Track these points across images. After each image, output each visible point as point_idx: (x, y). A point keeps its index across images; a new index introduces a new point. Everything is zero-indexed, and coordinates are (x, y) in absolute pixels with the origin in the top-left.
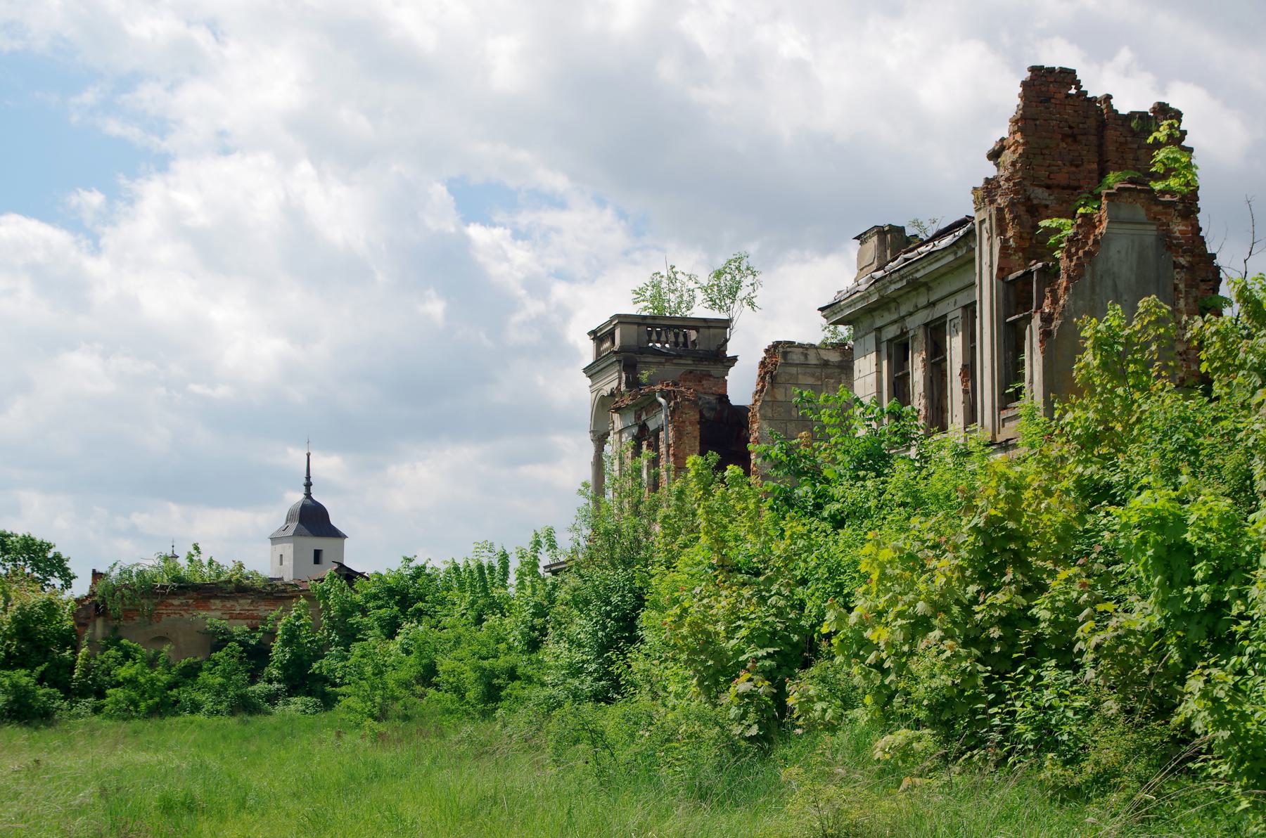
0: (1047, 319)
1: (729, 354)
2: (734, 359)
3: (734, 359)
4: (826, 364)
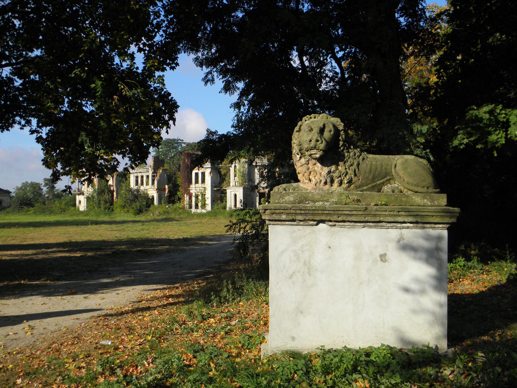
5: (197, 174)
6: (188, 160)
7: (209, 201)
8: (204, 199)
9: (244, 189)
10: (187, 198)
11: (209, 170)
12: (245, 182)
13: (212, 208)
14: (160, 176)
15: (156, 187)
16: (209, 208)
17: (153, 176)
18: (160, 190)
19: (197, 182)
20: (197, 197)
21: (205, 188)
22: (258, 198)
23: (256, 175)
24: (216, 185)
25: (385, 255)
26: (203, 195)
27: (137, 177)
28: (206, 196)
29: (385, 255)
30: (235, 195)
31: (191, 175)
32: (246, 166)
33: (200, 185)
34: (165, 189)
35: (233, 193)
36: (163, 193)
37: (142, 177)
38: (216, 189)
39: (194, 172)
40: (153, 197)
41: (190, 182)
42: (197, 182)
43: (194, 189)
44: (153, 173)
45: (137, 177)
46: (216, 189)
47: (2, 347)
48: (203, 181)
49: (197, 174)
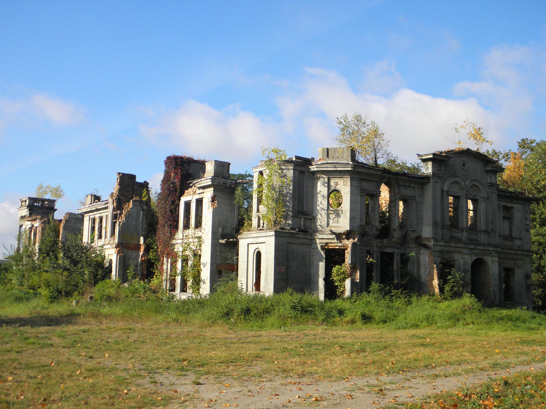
0: (120, 222)
1: (55, 208)
2: (56, 210)
3: (56, 210)
4: (78, 218)
5: (188, 205)
6: (176, 174)
7: (206, 274)
8: (197, 267)
9: (278, 235)
10: (166, 265)
11: (209, 194)
12: (286, 218)
13: (213, 289)
14: (127, 217)
15: (116, 241)
16: (205, 289)
17: (115, 217)
18: (125, 247)
19: (187, 226)
20: (185, 260)
21: (199, 238)
22: (322, 266)
23: (320, 199)
24: (228, 231)
25: (99, 200)
26: (197, 256)
27: (94, 220)
28: (202, 260)
29: (99, 200)
30: (259, 255)
31: (178, 205)
32: (290, 173)
33: (191, 232)
34: (139, 246)
35: (252, 248)
36: (134, 254)
37: (101, 219)
38: (223, 241)
39: (183, 199)
40: (111, 262)
41: (175, 227)
42: (187, 226)
43: (181, 240)
44: (114, 209)
45: (94, 220)
46: (223, 241)
47: (314, 399)
48: (198, 224)
49: (188, 205)
